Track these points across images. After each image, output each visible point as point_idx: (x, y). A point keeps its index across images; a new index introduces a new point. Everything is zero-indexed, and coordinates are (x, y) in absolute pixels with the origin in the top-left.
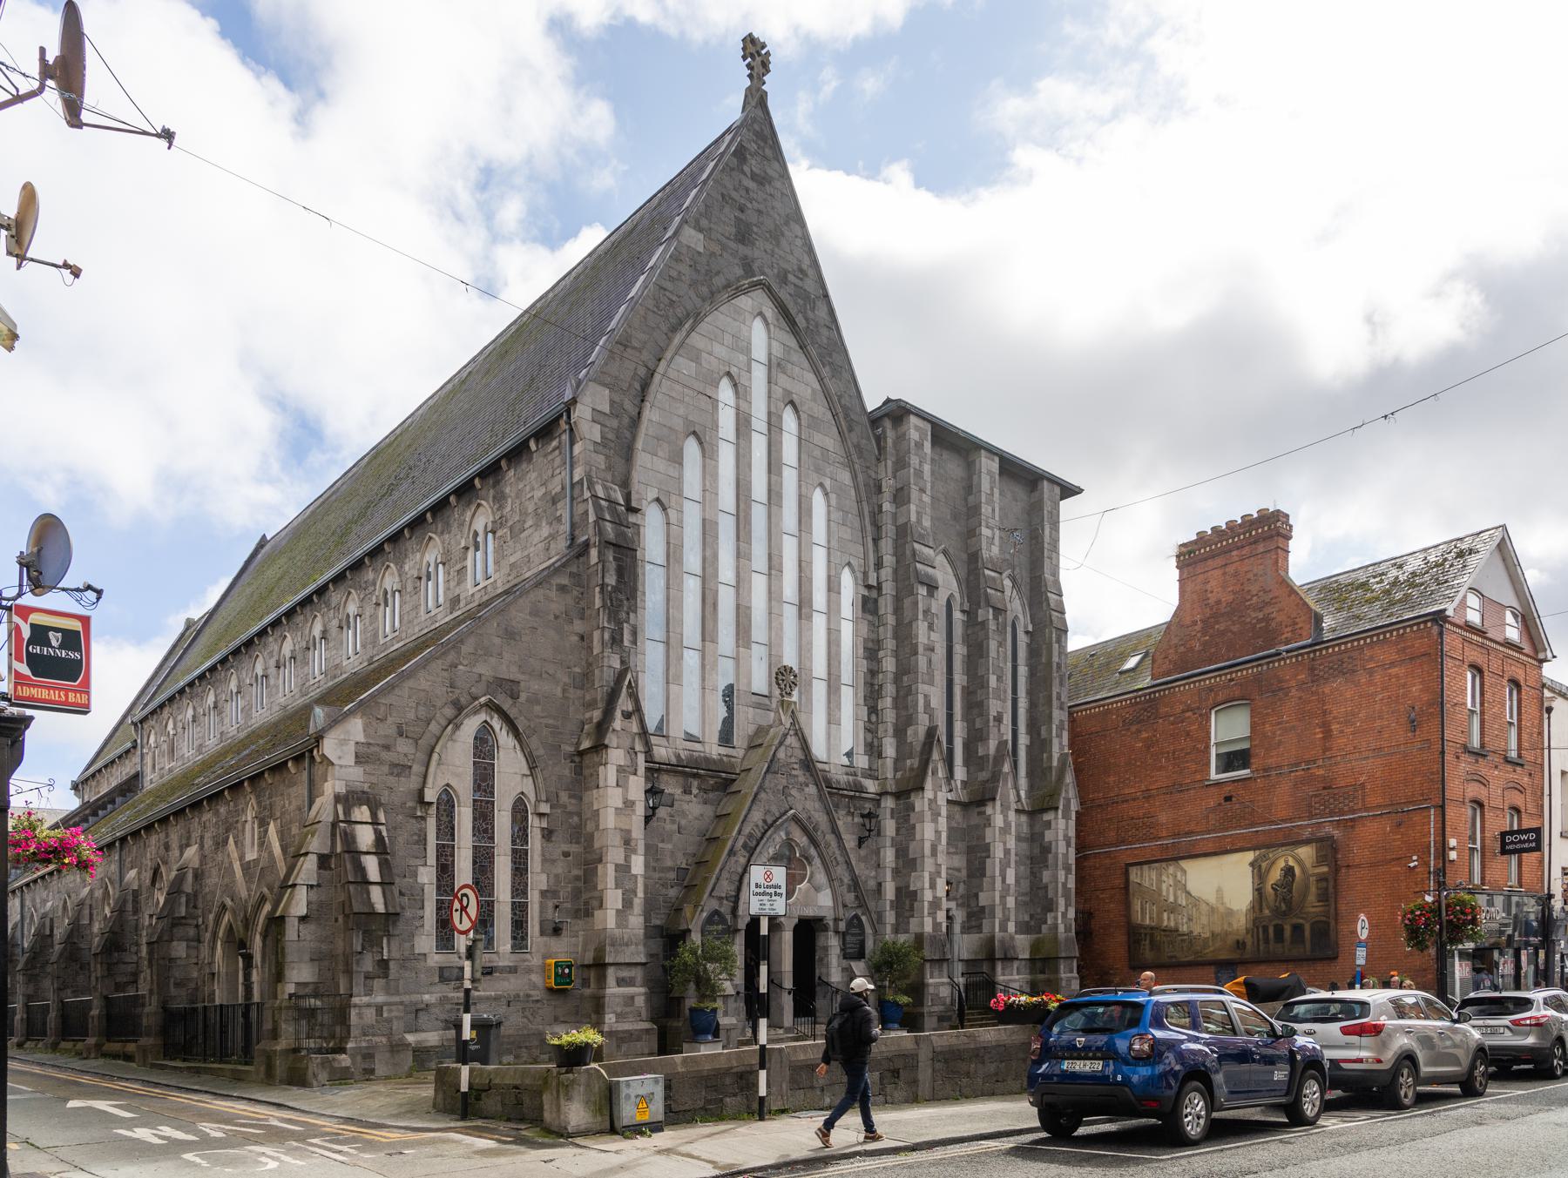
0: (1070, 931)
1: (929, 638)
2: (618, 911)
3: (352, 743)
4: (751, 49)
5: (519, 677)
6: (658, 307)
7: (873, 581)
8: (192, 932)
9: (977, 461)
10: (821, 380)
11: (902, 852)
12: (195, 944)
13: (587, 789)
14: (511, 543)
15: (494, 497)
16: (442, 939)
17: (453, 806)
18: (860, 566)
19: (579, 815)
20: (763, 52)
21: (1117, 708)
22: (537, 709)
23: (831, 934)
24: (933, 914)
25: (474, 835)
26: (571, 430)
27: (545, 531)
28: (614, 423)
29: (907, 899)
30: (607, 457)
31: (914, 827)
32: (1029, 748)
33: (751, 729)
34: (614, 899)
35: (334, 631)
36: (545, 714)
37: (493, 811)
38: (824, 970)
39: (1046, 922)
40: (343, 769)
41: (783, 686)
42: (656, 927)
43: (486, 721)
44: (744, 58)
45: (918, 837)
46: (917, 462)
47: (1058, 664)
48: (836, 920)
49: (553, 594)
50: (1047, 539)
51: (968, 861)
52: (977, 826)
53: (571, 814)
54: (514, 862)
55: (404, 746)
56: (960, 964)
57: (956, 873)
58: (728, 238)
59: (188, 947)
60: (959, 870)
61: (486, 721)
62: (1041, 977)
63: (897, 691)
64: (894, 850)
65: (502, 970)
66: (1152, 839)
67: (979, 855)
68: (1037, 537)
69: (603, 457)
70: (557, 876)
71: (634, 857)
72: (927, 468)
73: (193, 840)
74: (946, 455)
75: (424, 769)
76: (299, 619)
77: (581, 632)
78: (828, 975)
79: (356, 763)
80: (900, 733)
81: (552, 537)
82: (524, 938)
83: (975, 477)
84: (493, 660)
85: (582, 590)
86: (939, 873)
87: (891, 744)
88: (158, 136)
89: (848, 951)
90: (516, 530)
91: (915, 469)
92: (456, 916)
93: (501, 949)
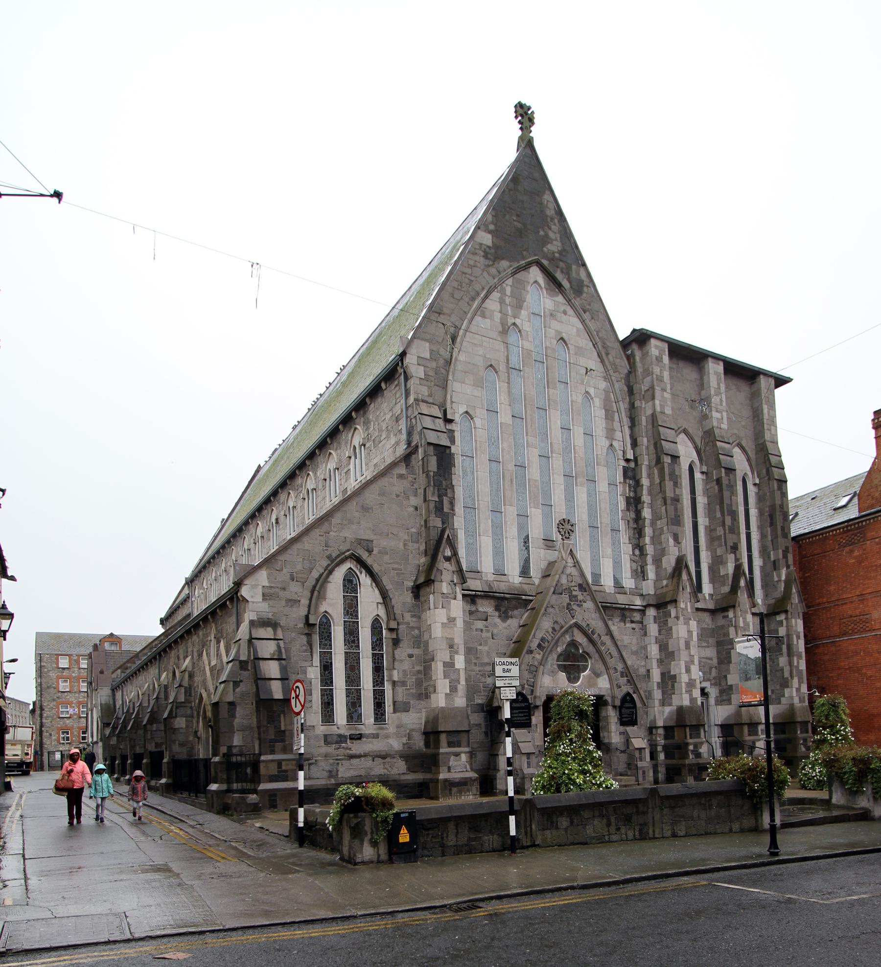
0: (804, 702)
1: (675, 491)
2: (446, 694)
3: (260, 587)
4: (521, 111)
5: (372, 537)
6: (461, 286)
7: (630, 455)
8: (189, 712)
9: (706, 366)
10: (583, 322)
11: (663, 647)
12: (190, 719)
13: (423, 611)
14: (374, 451)
15: (364, 423)
16: (326, 716)
17: (330, 626)
18: (620, 446)
19: (419, 628)
20: (529, 112)
21: (834, 535)
22: (386, 558)
23: (610, 708)
24: (689, 692)
25: (345, 645)
26: (405, 372)
27: (393, 440)
28: (434, 365)
29: (668, 681)
30: (429, 387)
31: (671, 629)
32: (762, 569)
33: (544, 565)
34: (443, 686)
35: (282, 518)
36: (392, 561)
37: (358, 628)
38: (606, 734)
39: (784, 696)
40: (255, 604)
41: (563, 533)
42: (478, 704)
43: (350, 568)
44: (516, 117)
45: (674, 636)
46: (658, 370)
47: (780, 505)
48: (613, 697)
49: (395, 480)
50: (766, 416)
51: (718, 652)
52: (723, 627)
53: (413, 628)
54: (374, 663)
55: (295, 588)
56: (716, 727)
57: (709, 661)
58: (510, 235)
59: (186, 720)
60: (711, 659)
61: (350, 568)
62: (782, 736)
63: (654, 532)
64: (658, 646)
65: (368, 736)
66: (866, 631)
67: (725, 647)
68: (758, 416)
69: (426, 388)
70: (404, 671)
71: (456, 657)
72: (666, 374)
73: (189, 654)
74: (681, 364)
75: (308, 602)
76: (265, 512)
77: (415, 505)
78: (609, 737)
79: (263, 599)
80: (657, 561)
81: (397, 443)
82: (383, 714)
83: (705, 378)
84: (354, 527)
85: (414, 476)
86: (692, 662)
87: (651, 570)
88: (51, 196)
89: (624, 719)
90: (377, 442)
91: (657, 375)
92: (293, 701)
93: (367, 722)
